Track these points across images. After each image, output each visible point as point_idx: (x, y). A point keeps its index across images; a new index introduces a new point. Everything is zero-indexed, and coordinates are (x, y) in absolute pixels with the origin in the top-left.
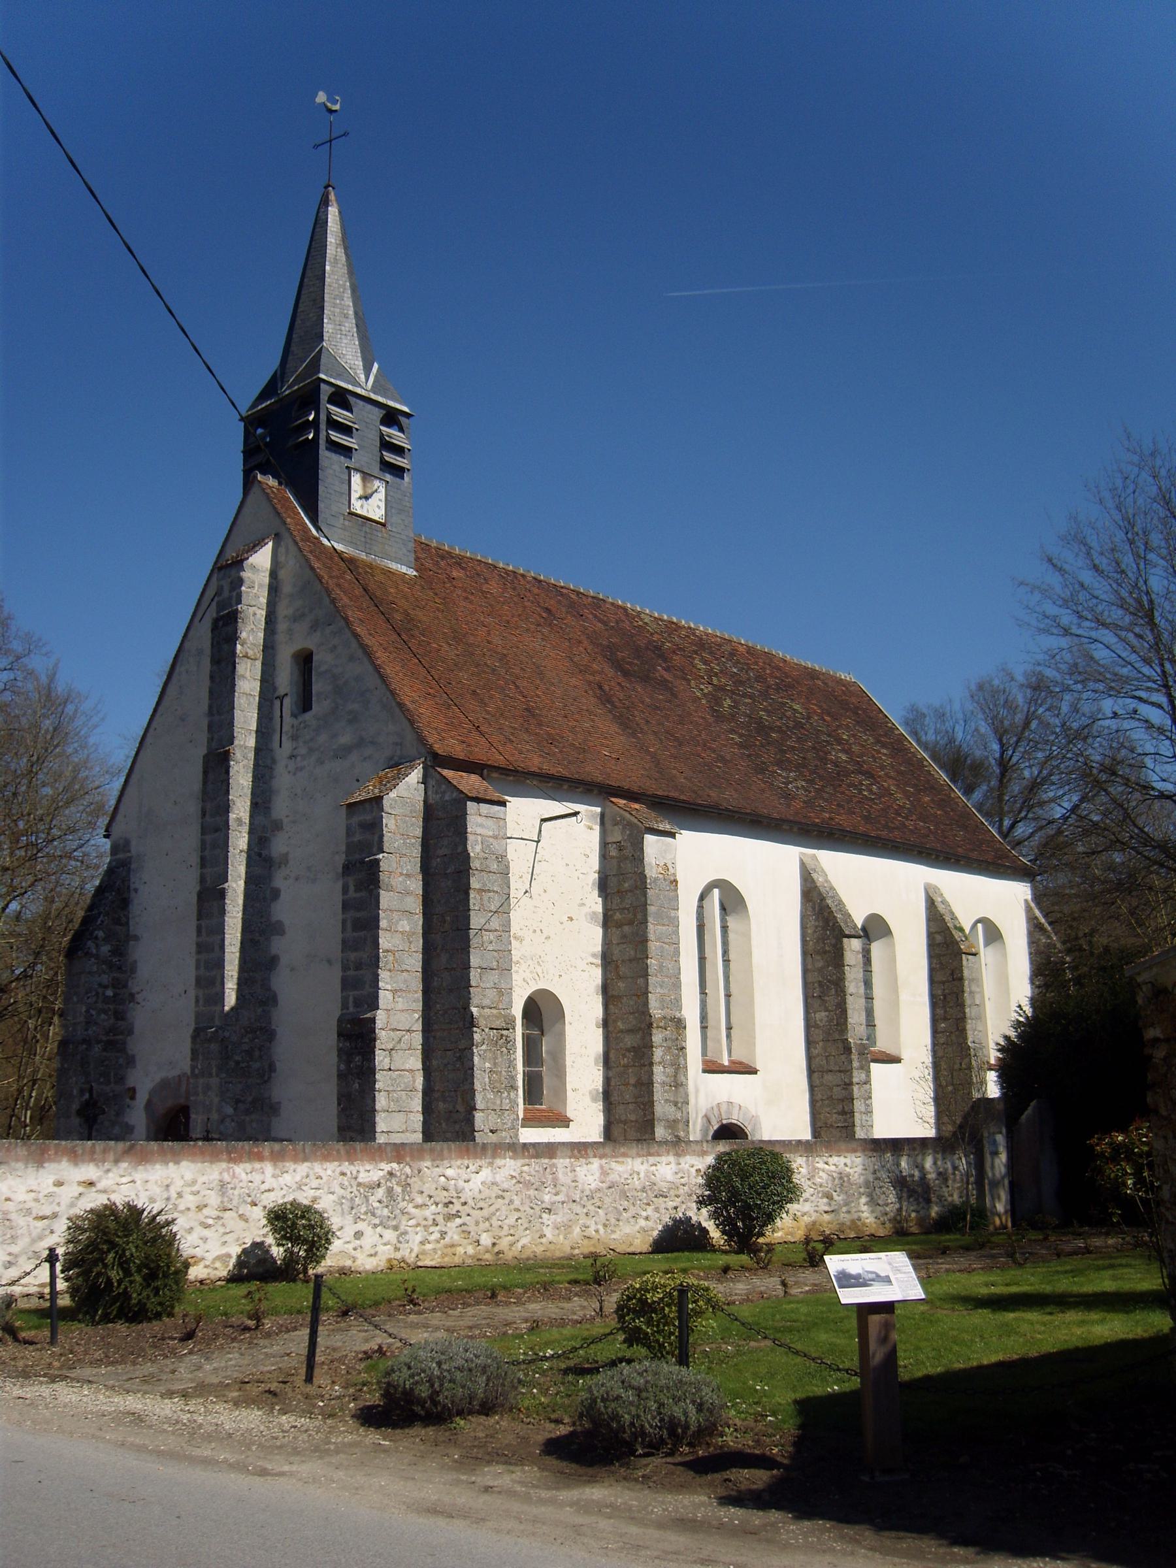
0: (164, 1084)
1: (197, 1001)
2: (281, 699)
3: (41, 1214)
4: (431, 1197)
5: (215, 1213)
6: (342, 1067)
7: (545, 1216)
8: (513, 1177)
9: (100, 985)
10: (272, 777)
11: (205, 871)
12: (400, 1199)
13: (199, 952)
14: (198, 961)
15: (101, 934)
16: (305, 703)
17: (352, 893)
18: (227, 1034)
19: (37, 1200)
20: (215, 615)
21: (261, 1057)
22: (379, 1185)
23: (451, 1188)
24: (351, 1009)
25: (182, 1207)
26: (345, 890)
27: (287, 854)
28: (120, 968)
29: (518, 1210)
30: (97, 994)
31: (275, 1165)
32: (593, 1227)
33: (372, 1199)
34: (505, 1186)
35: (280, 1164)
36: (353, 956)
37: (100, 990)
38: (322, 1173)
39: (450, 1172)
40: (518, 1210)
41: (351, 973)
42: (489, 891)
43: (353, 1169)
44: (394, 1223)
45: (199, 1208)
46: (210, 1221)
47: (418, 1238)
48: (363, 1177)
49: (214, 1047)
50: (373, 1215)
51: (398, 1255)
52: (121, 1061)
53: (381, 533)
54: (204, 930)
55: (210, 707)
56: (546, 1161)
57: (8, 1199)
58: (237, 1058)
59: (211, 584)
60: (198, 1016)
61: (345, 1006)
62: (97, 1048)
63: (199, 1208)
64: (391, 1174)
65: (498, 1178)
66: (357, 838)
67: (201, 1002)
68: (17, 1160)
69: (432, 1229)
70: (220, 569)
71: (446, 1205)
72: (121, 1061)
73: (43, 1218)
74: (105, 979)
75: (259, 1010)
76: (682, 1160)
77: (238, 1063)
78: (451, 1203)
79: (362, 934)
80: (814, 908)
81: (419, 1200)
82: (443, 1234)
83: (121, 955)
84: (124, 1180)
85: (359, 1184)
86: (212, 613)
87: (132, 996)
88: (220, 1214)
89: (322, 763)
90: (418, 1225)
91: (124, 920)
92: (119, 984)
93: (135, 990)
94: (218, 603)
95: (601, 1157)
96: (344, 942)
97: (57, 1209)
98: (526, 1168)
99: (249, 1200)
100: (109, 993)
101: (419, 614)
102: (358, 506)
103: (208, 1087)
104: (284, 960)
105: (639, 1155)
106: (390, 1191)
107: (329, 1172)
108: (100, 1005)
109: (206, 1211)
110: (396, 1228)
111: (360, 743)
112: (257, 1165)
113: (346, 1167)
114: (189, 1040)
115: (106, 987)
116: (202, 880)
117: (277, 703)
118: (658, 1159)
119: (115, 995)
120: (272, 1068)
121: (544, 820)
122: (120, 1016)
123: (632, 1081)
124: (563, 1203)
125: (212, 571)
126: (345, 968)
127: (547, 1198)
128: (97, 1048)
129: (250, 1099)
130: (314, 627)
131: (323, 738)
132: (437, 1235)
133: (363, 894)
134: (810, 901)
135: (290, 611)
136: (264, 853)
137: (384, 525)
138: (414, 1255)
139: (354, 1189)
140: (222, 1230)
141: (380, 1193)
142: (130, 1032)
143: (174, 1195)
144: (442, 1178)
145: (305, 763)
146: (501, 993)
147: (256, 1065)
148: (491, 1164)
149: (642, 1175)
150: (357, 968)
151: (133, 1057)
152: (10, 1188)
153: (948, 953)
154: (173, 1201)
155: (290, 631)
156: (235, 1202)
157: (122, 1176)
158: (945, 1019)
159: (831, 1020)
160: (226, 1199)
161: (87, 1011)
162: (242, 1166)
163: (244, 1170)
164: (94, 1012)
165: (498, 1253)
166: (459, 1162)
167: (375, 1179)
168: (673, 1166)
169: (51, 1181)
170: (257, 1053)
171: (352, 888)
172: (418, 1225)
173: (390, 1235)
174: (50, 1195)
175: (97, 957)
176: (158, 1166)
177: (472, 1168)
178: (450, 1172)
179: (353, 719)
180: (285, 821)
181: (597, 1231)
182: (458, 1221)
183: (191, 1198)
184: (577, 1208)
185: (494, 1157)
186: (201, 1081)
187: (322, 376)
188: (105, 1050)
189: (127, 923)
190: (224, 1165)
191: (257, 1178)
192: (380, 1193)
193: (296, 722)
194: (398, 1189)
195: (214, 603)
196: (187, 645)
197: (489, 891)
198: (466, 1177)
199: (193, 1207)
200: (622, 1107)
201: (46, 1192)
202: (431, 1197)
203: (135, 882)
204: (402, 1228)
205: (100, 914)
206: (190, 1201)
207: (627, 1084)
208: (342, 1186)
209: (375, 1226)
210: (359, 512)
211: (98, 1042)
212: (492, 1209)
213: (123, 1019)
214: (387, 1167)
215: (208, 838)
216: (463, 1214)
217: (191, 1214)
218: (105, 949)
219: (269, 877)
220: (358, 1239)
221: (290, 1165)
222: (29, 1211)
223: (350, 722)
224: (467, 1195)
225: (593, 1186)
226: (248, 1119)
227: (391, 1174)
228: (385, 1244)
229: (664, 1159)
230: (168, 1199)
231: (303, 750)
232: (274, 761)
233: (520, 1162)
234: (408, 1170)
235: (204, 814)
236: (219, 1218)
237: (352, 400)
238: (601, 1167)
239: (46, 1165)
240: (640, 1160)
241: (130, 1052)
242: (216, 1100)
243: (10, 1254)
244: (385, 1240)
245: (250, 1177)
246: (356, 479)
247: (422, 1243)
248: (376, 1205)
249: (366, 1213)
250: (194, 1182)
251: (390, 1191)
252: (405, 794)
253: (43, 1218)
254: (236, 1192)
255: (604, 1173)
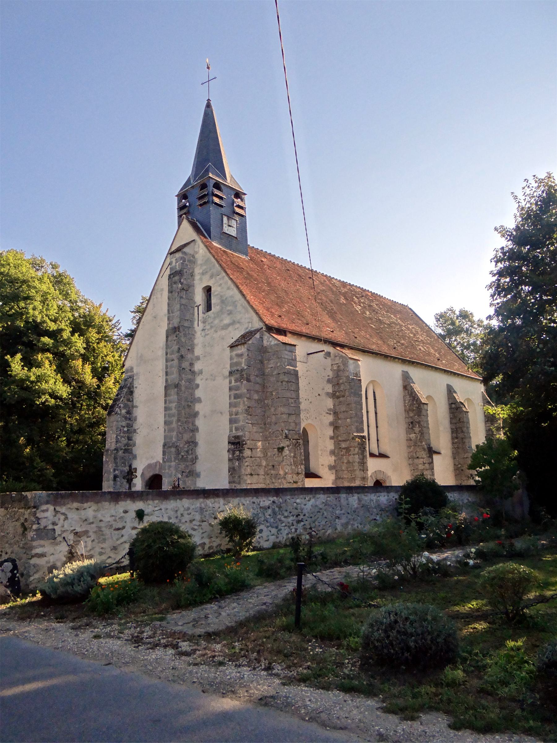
0: (149, 466)
1: (165, 430)
2: (198, 307)
3: (117, 527)
4: (290, 512)
5: (198, 523)
6: (231, 456)
7: (337, 520)
8: (323, 503)
9: (122, 426)
10: (195, 339)
11: (167, 377)
12: (278, 514)
13: (165, 411)
14: (165, 415)
15: (122, 405)
16: (209, 307)
17: (233, 383)
18: (178, 444)
19: (115, 520)
20: (169, 273)
21: (192, 453)
22: (269, 508)
23: (299, 508)
24: (234, 432)
25: (183, 521)
26: (230, 382)
27: (202, 370)
28: (130, 419)
29: (326, 518)
30: (120, 430)
31: (224, 500)
32: (356, 525)
33: (266, 514)
34: (321, 506)
35: (227, 499)
36: (234, 410)
37: (122, 428)
38: (244, 503)
39: (298, 501)
40: (326, 518)
41: (233, 416)
42: (291, 382)
43: (258, 500)
44: (276, 525)
45: (191, 521)
46: (196, 527)
47: (286, 532)
48: (262, 504)
49: (173, 450)
50: (267, 521)
51: (278, 540)
52: (130, 457)
53: (234, 241)
54: (168, 402)
55: (168, 311)
56: (337, 495)
57: (101, 521)
58: (183, 454)
59: (166, 262)
60: (165, 437)
61: (231, 430)
62: (121, 452)
63: (191, 521)
64: (274, 502)
65: (318, 503)
66: (235, 361)
67: (167, 432)
68: (106, 501)
69: (292, 527)
70: (171, 254)
71: (297, 516)
72: (130, 457)
73: (118, 529)
74: (124, 424)
75: (191, 434)
76: (389, 495)
77: (183, 456)
78: (299, 515)
79: (238, 400)
80: (408, 393)
81: (286, 514)
82: (296, 530)
83: (130, 414)
84: (156, 509)
85: (261, 507)
86: (168, 272)
87: (135, 431)
88: (201, 524)
89: (217, 332)
90: (286, 526)
91: (131, 399)
92: (129, 426)
93: (136, 428)
94: (170, 268)
95: (358, 493)
96: (230, 403)
97: (125, 524)
98: (328, 499)
99: (213, 516)
100: (126, 429)
101: (253, 273)
102: (226, 229)
103: (170, 467)
104: (201, 413)
105: (373, 493)
106: (274, 509)
107: (248, 502)
108: (122, 434)
109: (194, 523)
110: (277, 527)
111: (233, 323)
112: (217, 500)
113: (255, 499)
114: (162, 447)
115: (124, 427)
116: (167, 381)
117: (197, 308)
118: (380, 494)
119: (128, 430)
120: (196, 458)
121: (308, 354)
122: (130, 439)
123: (345, 461)
124: (344, 514)
125: (168, 254)
126: (231, 415)
127: (337, 512)
128: (121, 452)
129: (188, 471)
130: (212, 277)
131: (216, 322)
132: (293, 530)
133: (238, 383)
134: (406, 390)
135: (201, 271)
136: (192, 370)
137: (236, 238)
138: (284, 540)
139: (259, 510)
140: (201, 531)
141: (270, 511)
142: (134, 445)
143: (179, 515)
144: (295, 504)
145: (209, 332)
146: (296, 424)
147: (190, 457)
148: (314, 497)
149: (374, 501)
150: (236, 415)
151: (136, 455)
152: (102, 515)
153: (456, 410)
154: (179, 518)
155: (201, 279)
156: (207, 518)
157: (155, 507)
158: (457, 438)
159: (417, 437)
160: (203, 516)
161: (117, 437)
162: (210, 500)
163: (211, 502)
164: (119, 437)
165: (319, 538)
166: (301, 496)
167: (267, 504)
168: (386, 497)
169: (122, 511)
170: (190, 452)
171: (233, 381)
172: (286, 526)
173: (274, 531)
174: (121, 518)
175: (120, 414)
176: (172, 501)
177: (307, 499)
178: (298, 501)
179: (230, 313)
180: (201, 356)
181: (358, 527)
182: (302, 523)
183: (188, 516)
184: (350, 516)
185: (316, 494)
186: (167, 464)
187: (211, 175)
188: (124, 453)
189: (133, 401)
190: (201, 500)
191: (217, 505)
192: (270, 511)
193: (205, 316)
194: (277, 509)
195: (169, 268)
196: (156, 287)
197: (291, 382)
198: (305, 503)
199: (188, 520)
200: (341, 472)
201: (119, 517)
202: (290, 512)
203: (136, 384)
204: (279, 527)
205: (121, 397)
206: (187, 518)
207: (343, 463)
208: (253, 508)
209: (268, 527)
210: (227, 232)
211: (121, 449)
212: (316, 517)
213: (131, 440)
214: (272, 499)
215: (169, 364)
216: (304, 520)
217: (187, 524)
218: (124, 411)
219: (194, 380)
220: (261, 533)
221: (231, 499)
222: (111, 526)
223: (229, 314)
224: (305, 511)
225: (356, 506)
226: (187, 479)
227: (274, 502)
228: (272, 535)
229: (382, 494)
230: (177, 517)
231: (208, 327)
232: (195, 332)
233: (326, 496)
234: (281, 500)
235: (167, 354)
236: (200, 525)
237: (222, 186)
238: (358, 498)
239: (120, 503)
240: (373, 495)
241: (134, 453)
242: (174, 472)
243: (102, 548)
244: (272, 533)
245: (213, 505)
246: (225, 219)
247: (287, 534)
248: (268, 517)
249: (264, 521)
250: (189, 509)
251: (274, 509)
252: (255, 342)
253: (118, 529)
254: (208, 513)
255: (359, 500)
